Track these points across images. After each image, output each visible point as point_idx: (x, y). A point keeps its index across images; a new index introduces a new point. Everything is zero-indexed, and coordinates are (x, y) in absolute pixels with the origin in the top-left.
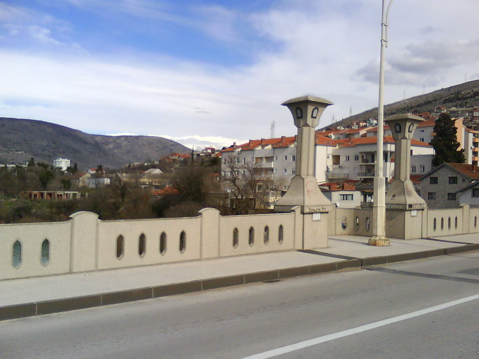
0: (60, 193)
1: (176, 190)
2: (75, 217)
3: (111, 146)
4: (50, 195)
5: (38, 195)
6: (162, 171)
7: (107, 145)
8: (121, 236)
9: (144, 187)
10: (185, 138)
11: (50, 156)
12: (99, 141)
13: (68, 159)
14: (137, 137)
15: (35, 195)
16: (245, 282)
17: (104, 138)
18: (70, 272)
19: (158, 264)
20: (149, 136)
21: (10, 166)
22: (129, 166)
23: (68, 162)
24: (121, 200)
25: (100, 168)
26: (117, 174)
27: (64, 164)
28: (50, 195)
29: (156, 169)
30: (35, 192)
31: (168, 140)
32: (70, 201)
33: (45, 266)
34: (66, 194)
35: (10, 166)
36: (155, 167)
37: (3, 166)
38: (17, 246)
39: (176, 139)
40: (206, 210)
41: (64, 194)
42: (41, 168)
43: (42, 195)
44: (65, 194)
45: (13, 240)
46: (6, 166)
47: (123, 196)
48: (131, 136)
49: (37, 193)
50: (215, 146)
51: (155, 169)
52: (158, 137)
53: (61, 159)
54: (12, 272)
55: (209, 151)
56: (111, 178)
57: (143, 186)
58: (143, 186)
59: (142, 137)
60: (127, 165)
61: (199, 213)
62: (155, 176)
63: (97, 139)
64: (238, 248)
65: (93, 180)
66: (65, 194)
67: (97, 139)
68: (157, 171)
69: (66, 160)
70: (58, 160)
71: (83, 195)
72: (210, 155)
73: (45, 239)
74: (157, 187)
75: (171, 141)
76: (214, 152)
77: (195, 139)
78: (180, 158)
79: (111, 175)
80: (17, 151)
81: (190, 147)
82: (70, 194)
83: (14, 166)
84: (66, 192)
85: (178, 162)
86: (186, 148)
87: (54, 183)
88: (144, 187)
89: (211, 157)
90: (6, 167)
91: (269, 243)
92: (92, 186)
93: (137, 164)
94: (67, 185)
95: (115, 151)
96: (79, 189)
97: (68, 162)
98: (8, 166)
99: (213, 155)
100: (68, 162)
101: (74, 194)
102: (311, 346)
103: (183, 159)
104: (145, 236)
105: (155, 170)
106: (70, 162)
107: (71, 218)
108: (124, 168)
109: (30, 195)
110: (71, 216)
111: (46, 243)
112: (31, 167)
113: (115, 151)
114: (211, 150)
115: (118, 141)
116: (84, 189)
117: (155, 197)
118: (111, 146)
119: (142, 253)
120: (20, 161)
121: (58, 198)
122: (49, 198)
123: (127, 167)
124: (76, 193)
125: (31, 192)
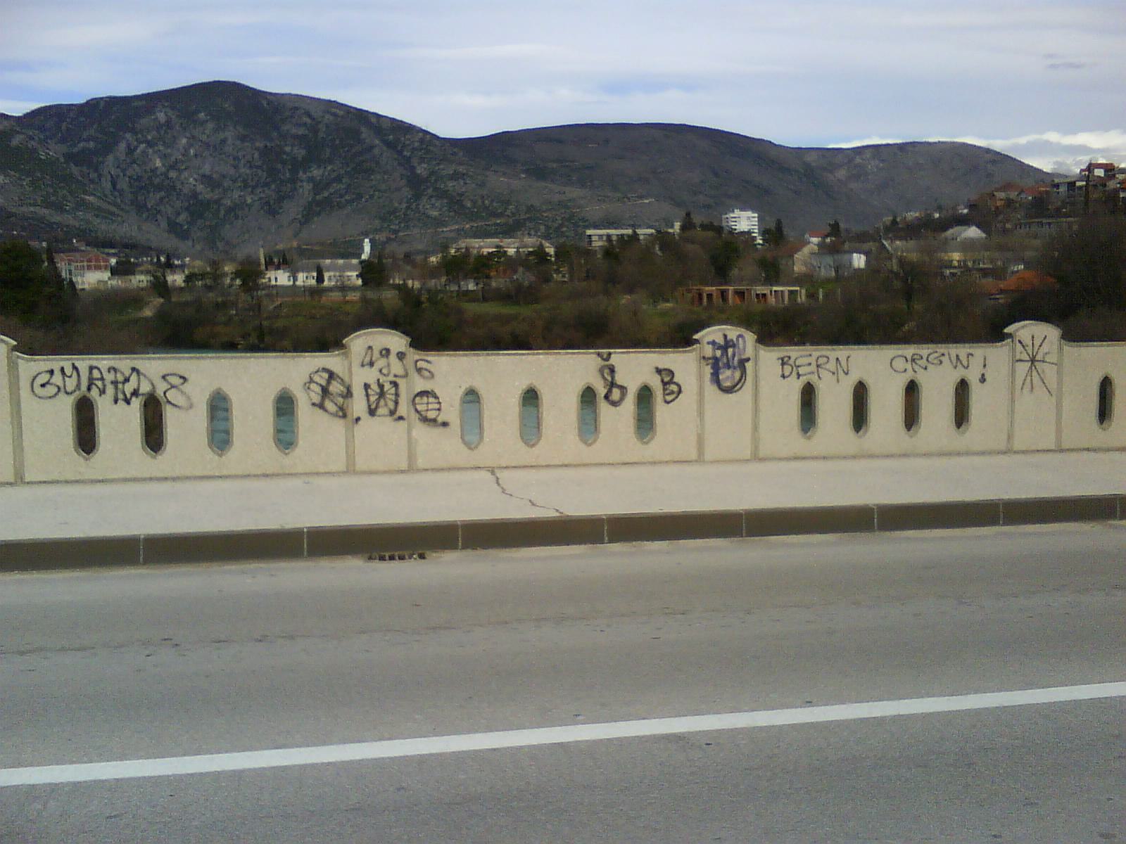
0: (761, 289)
1: (1052, 280)
2: (352, 344)
3: (841, 174)
4: (741, 294)
5: (715, 297)
6: (984, 232)
7: (831, 172)
8: (646, 386)
9: (951, 273)
10: (1023, 140)
11: (708, 207)
12: (814, 164)
13: (753, 213)
14: (902, 147)
15: (710, 296)
16: (141, 560)
17: (824, 156)
18: (411, 469)
19: (450, 469)
20: (931, 140)
21: (643, 232)
22: (894, 222)
23: (754, 217)
24: (905, 306)
25: (835, 229)
26: (883, 244)
27: (745, 221)
28: (741, 294)
29: (969, 227)
30: (710, 288)
31: (980, 147)
32: (786, 309)
33: (809, 438)
34: (775, 291)
35: (643, 232)
36: (964, 221)
37: (629, 231)
38: (531, 397)
39: (998, 145)
40: (1023, 327)
41: (771, 291)
42: (710, 234)
43: (723, 294)
44: (773, 293)
45: (524, 386)
46: (635, 232)
47: (908, 295)
48: (888, 145)
49: (713, 291)
50: (1103, 157)
51: (964, 228)
52: (954, 143)
53: (737, 213)
54: (799, 443)
55: (1099, 173)
56: (867, 254)
57: (948, 272)
58: (948, 272)
59: (914, 147)
60: (888, 219)
61: (695, 339)
62: (968, 246)
63: (808, 159)
64: (233, 453)
65: (829, 260)
66: (773, 293)
67: (810, 158)
68: (973, 232)
69: (749, 214)
70: (732, 215)
71: (812, 296)
72: (1102, 182)
73: (584, 387)
74: (985, 273)
75: (988, 151)
76: (1114, 175)
77: (1047, 143)
78: (1023, 196)
79: (866, 246)
80: (641, 197)
81: (1044, 164)
82: (782, 291)
83: (652, 231)
84: (775, 288)
85: (1018, 205)
86: (1028, 166)
87: (744, 269)
88: (951, 273)
89: (1107, 189)
90: (635, 235)
91: (869, 434)
92: (827, 272)
93: (912, 215)
94: (772, 271)
95: (853, 185)
96: (799, 280)
97: (754, 219)
98: (639, 231)
99: (1112, 185)
100: (754, 217)
101: (791, 292)
102: (874, 718)
103: (1030, 198)
104: (1111, 383)
105: (965, 230)
106: (756, 219)
107: (697, 341)
108: (882, 228)
109: (700, 295)
110: (696, 337)
111: (1106, 387)
112: (688, 234)
113: (853, 185)
114: (1102, 171)
115: (858, 160)
116: (807, 280)
117: (990, 299)
118: (841, 174)
119: (860, 429)
120: (649, 220)
121: (759, 302)
122: (738, 301)
123: (888, 223)
124: (797, 291)
125: (699, 290)
